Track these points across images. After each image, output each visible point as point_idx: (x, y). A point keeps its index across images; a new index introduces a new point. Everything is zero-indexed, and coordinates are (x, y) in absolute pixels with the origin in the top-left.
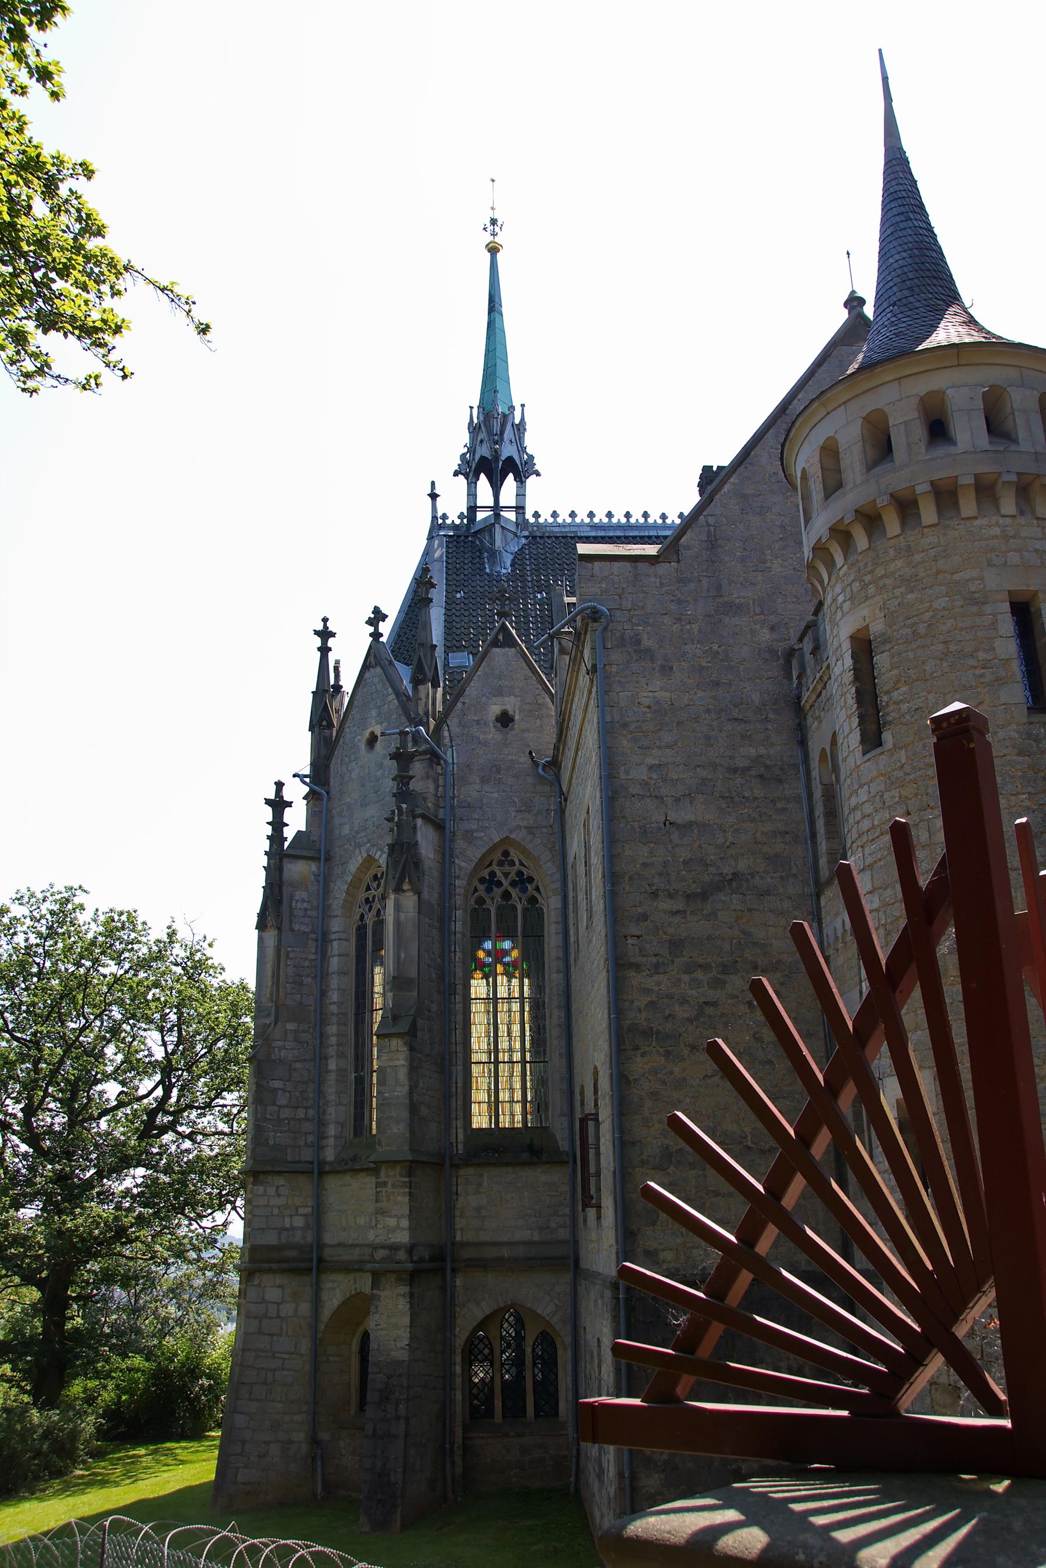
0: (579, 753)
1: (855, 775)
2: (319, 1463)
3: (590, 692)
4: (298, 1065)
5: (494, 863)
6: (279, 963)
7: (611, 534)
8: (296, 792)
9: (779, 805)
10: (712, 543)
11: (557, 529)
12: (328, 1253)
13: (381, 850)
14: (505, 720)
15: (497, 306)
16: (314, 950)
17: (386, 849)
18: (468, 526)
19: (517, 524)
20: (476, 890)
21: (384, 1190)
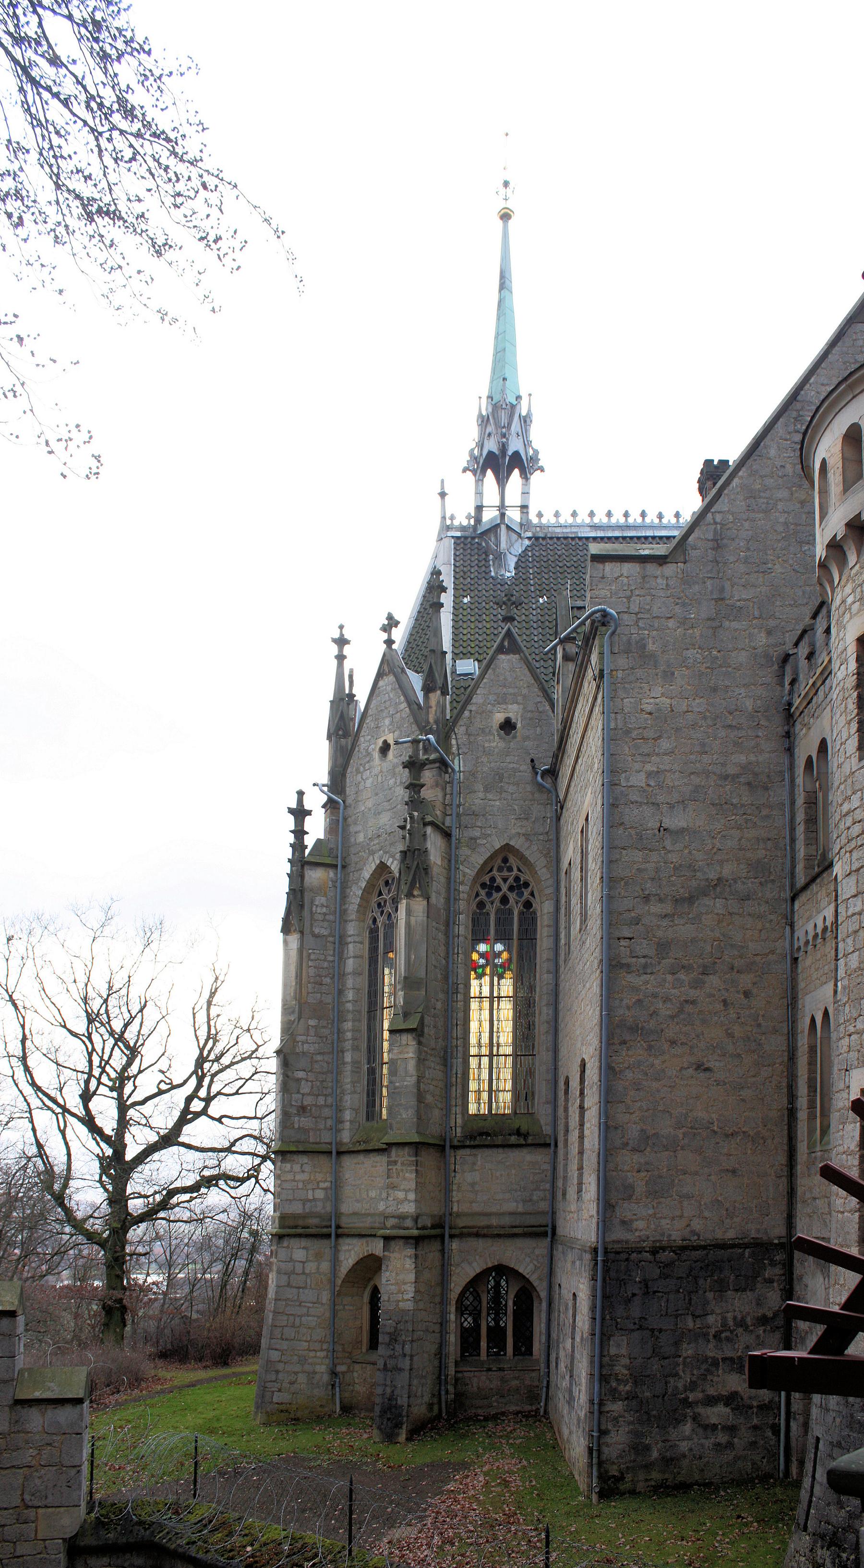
0: (580, 761)
1: (849, 781)
2: (337, 1389)
3: (595, 698)
4: (319, 1058)
5: (495, 869)
6: (301, 965)
7: (610, 534)
8: (315, 801)
9: (765, 812)
10: (718, 544)
11: (558, 530)
12: (344, 1221)
13: (393, 857)
14: (508, 726)
15: (507, 282)
16: (331, 952)
17: (398, 856)
18: (475, 528)
19: (521, 525)
20: (477, 895)
21: (394, 1168)
